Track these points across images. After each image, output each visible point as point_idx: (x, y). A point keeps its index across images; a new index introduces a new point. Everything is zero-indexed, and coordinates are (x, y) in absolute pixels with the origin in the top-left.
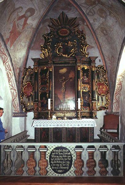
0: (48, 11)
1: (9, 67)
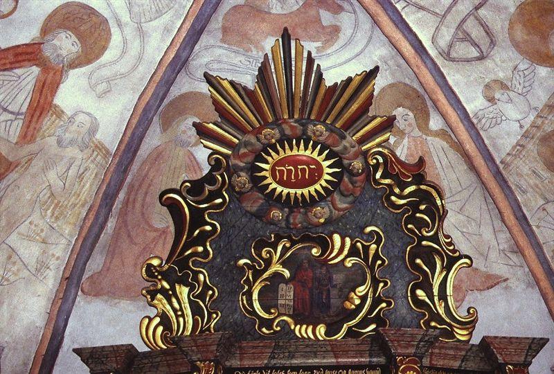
0: (195, 34)
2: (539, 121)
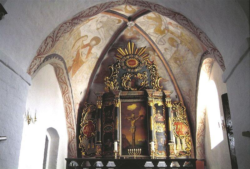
1: (68, 99)
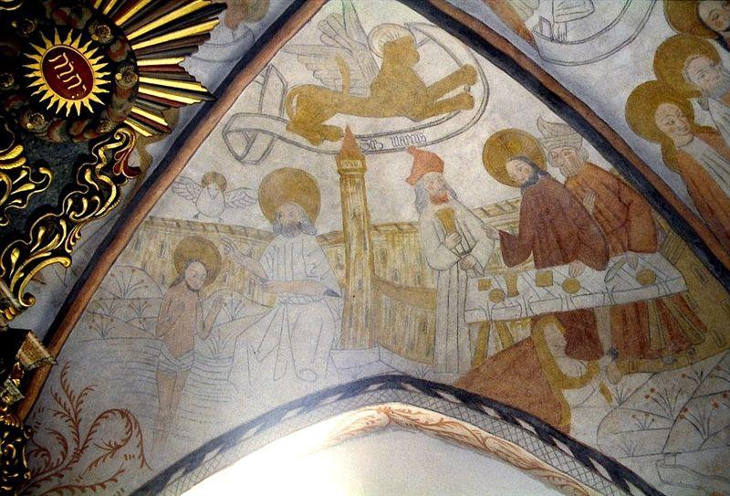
2: (210, 228)
